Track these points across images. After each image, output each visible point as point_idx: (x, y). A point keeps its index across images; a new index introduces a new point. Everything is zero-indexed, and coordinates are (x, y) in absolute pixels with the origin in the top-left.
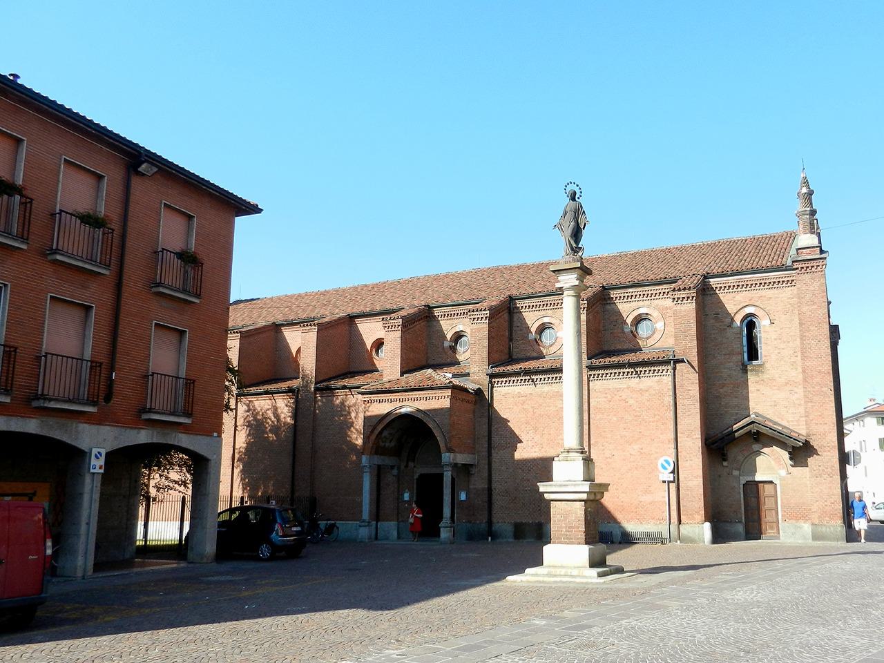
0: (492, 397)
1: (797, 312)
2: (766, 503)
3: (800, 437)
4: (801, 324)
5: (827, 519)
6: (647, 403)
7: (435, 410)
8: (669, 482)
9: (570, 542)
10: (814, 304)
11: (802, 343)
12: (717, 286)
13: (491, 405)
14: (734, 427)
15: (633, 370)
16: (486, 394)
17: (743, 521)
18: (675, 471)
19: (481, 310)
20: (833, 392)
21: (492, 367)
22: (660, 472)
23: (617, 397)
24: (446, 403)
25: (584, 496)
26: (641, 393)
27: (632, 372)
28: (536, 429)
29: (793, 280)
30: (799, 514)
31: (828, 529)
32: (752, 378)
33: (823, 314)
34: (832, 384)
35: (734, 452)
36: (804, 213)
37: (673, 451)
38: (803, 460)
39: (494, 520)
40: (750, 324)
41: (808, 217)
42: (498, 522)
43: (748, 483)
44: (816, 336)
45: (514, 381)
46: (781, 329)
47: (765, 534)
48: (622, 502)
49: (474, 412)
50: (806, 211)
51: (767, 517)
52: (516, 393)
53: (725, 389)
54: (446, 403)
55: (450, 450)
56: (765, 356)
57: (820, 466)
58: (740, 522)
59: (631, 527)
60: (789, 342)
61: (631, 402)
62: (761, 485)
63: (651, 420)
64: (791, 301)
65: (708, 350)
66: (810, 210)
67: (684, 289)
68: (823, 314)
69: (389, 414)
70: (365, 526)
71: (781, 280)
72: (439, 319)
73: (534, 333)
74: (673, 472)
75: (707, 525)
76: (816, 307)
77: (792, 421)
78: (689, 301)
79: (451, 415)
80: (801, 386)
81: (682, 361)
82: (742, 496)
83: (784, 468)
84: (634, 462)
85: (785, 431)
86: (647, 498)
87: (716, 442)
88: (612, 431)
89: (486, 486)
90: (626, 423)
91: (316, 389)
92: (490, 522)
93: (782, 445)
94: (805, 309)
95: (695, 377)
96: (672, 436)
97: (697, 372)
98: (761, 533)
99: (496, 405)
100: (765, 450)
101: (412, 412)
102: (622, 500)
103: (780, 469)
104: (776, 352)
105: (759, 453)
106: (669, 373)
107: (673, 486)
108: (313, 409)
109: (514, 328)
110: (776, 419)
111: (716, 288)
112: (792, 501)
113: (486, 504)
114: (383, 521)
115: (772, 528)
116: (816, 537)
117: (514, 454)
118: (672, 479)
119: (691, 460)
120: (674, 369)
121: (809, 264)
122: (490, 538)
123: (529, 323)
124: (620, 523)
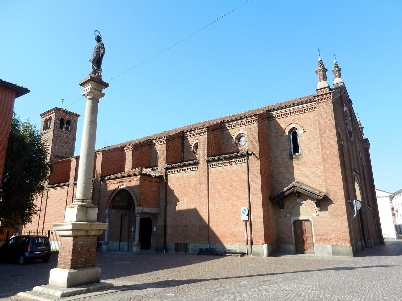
0: (167, 179)
1: (318, 124)
2: (307, 232)
3: (321, 193)
4: (320, 130)
7: (134, 186)
8: (246, 221)
9: (63, 268)
10: (327, 118)
11: (321, 141)
13: (167, 183)
14: (284, 189)
15: (228, 161)
16: (164, 178)
17: (294, 243)
18: (249, 215)
19: (163, 138)
21: (167, 165)
22: (242, 216)
23: (221, 176)
24: (137, 183)
25: (71, 233)
26: (232, 173)
27: (228, 162)
28: (185, 194)
29: (315, 107)
30: (324, 240)
31: (342, 249)
32: (295, 162)
33: (332, 123)
34: (340, 163)
35: (288, 204)
36: (319, 71)
37: (248, 203)
38: (325, 207)
39: (167, 241)
40: (294, 132)
41: (322, 72)
43: (295, 221)
44: (329, 136)
45: (176, 171)
47: (307, 250)
48: (224, 232)
49: (159, 187)
50: (321, 69)
51: (308, 242)
52: (177, 177)
53: (282, 169)
54: (137, 183)
55: (139, 206)
56: (302, 150)
58: (292, 243)
59: (229, 246)
61: (228, 178)
62: (303, 222)
64: (315, 119)
65: (272, 149)
66: (323, 69)
67: (251, 116)
68: (332, 123)
69: (116, 189)
70: (105, 244)
71: (308, 108)
72: (155, 145)
73: (192, 148)
74: (248, 215)
75: (265, 245)
76: (327, 120)
77: (318, 185)
78: (255, 122)
79: (140, 189)
80: (322, 165)
81: (250, 155)
82: (293, 228)
83: (315, 212)
84: (229, 210)
85: (312, 191)
86: (236, 230)
87: (275, 198)
89: (164, 224)
90: (226, 189)
91: (101, 180)
92: (165, 243)
93: (312, 199)
94: (322, 121)
95: (258, 162)
96: (247, 195)
97: (259, 160)
98: (304, 250)
99: (169, 183)
100: (304, 202)
102: (224, 231)
103: (313, 213)
104: (308, 147)
105: (301, 204)
106: (245, 161)
107: (248, 223)
108: (99, 189)
109: (185, 146)
110: (309, 184)
111: (275, 116)
112: (320, 231)
114: (122, 241)
115: (310, 247)
116: (335, 253)
118: (247, 219)
119: (257, 209)
120: (248, 159)
121: (323, 97)
122: (165, 251)
123: (191, 143)
124: (223, 244)
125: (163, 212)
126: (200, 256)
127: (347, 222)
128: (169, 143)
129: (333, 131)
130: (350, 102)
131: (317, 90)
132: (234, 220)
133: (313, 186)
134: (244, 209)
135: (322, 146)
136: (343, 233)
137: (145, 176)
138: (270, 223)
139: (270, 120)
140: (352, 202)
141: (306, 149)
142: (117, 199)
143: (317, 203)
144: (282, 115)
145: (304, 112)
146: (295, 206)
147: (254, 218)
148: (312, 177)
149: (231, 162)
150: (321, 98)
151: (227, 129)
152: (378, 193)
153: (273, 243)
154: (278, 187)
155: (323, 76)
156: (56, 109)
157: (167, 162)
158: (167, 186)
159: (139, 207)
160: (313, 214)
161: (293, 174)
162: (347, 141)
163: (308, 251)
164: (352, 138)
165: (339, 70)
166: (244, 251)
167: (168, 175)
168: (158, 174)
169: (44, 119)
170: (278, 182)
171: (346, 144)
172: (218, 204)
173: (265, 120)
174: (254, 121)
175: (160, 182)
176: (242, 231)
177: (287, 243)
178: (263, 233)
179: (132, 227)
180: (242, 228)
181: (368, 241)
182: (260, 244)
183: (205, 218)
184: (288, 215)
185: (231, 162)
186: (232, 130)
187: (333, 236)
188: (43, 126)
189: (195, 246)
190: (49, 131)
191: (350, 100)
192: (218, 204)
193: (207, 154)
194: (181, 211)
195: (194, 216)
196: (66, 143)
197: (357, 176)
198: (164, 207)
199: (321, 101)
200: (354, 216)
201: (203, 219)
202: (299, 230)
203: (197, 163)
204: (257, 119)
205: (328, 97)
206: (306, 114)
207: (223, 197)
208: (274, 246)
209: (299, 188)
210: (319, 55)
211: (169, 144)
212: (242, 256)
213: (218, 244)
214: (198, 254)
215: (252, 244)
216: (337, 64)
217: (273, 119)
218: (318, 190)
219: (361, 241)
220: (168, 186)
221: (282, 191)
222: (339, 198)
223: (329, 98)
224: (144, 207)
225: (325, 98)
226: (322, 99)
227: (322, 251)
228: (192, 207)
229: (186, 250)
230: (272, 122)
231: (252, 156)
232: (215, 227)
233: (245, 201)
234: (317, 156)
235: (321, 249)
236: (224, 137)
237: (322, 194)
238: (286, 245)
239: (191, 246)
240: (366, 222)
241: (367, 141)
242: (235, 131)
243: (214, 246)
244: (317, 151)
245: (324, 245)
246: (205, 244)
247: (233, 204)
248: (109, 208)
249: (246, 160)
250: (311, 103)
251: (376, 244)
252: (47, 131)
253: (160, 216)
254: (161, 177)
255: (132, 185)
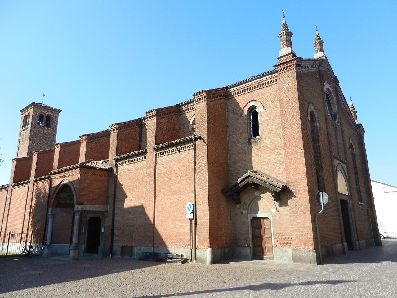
2: (266, 233)
4: (281, 106)
5: (303, 245)
6: (182, 168)
8: (191, 219)
10: (289, 91)
11: (282, 119)
12: (234, 92)
13: (116, 177)
15: (176, 148)
16: (114, 170)
17: (251, 246)
18: (194, 212)
20: (303, 150)
27: (175, 149)
29: (276, 80)
30: (284, 242)
31: (303, 254)
32: (254, 147)
35: (245, 198)
36: (282, 35)
37: (193, 198)
39: (114, 244)
40: (253, 112)
41: (285, 37)
42: (115, 245)
44: (291, 113)
46: (271, 112)
47: (265, 256)
48: (169, 233)
49: (108, 181)
50: (283, 33)
51: (267, 245)
52: (126, 169)
55: (79, 203)
57: (296, 205)
58: (249, 246)
59: (173, 250)
60: (275, 120)
63: (184, 178)
66: (286, 32)
69: (59, 185)
74: (193, 212)
75: (209, 249)
76: (290, 93)
78: (204, 100)
79: (80, 184)
82: (250, 228)
84: (175, 206)
85: (269, 181)
86: (181, 231)
87: (229, 191)
88: (166, 187)
89: (111, 224)
90: (172, 182)
92: (112, 245)
94: (283, 96)
96: (193, 188)
100: (263, 195)
101: (67, 183)
105: (259, 198)
107: (194, 221)
110: (269, 173)
111: (233, 94)
113: (110, 235)
115: (269, 251)
116: (296, 259)
117: (123, 205)
118: (192, 217)
120: (195, 145)
122: (111, 255)
125: (111, 209)
126: (142, 262)
127: (310, 220)
128: (122, 131)
129: (295, 107)
130: (336, 80)
131: (278, 58)
132: (179, 219)
133: (273, 175)
134: (189, 205)
135: (283, 126)
136: (306, 233)
137: (87, 168)
138: (222, 222)
139: (228, 99)
140: (319, 194)
141: (266, 131)
142: (62, 195)
143: (275, 196)
144: (240, 91)
145: (265, 86)
146: (252, 201)
147: (199, 216)
148: (272, 165)
149: (178, 149)
150: (283, 67)
151: (184, 113)
152: (374, 185)
153: (226, 246)
154: (234, 177)
155: (287, 40)
156: (34, 104)
157: (118, 152)
158: (116, 180)
159: (78, 204)
160: (273, 210)
161: (251, 161)
162: (326, 123)
163: (267, 256)
164: (337, 122)
165: (321, 43)
166: (188, 255)
167: (118, 168)
168: (107, 166)
169: (24, 115)
170: (235, 172)
171: (324, 127)
172: (164, 199)
173: (222, 99)
174: (203, 98)
175: (109, 176)
176: (187, 231)
177: (243, 246)
178: (208, 234)
179: (83, 228)
180: (187, 228)
181: (356, 243)
182: (205, 247)
183: (151, 216)
184: (245, 212)
185: (178, 149)
186: (189, 114)
187: (294, 237)
188: (22, 123)
189: (140, 250)
190: (28, 128)
191: (336, 78)
192: (164, 199)
193: (155, 142)
194: (128, 209)
195: (140, 215)
196: (45, 140)
197: (341, 165)
198: (112, 205)
199: (283, 71)
200: (320, 213)
201: (148, 218)
202: (257, 230)
203: (145, 152)
204: (206, 95)
205: (291, 66)
206: (267, 88)
207: (170, 191)
208: (227, 250)
209: (255, 178)
210: (283, 16)
211: (121, 133)
212: (184, 262)
213: (162, 247)
214: (140, 260)
215: (196, 248)
216: (319, 36)
217: (232, 97)
218: (277, 180)
219: (342, 243)
220: (117, 181)
221: (236, 182)
222: (302, 189)
223: (292, 66)
224: (85, 204)
225: (287, 67)
226: (284, 68)
227: (282, 256)
228: (139, 204)
229: (131, 254)
230: (230, 101)
231: (201, 140)
232: (161, 228)
233: (191, 195)
234: (278, 138)
235: (281, 253)
236: (181, 122)
237: (280, 185)
238: (242, 249)
239: (136, 250)
240: (354, 220)
241: (360, 126)
242: (192, 114)
243: (157, 250)
244: (278, 132)
245: (284, 249)
246: (149, 248)
247: (179, 199)
248: (53, 206)
249: (194, 146)
250: (272, 75)
251: (369, 245)
252: (25, 128)
253: (108, 215)
254: (110, 170)
255: (73, 180)
